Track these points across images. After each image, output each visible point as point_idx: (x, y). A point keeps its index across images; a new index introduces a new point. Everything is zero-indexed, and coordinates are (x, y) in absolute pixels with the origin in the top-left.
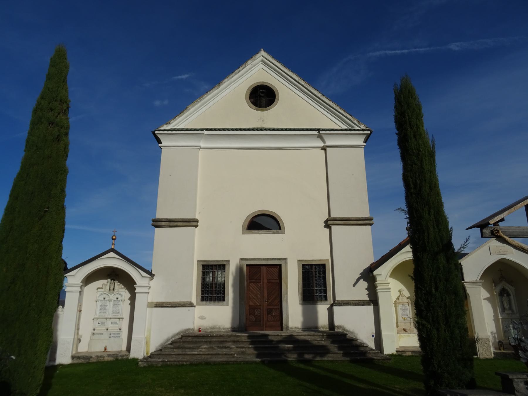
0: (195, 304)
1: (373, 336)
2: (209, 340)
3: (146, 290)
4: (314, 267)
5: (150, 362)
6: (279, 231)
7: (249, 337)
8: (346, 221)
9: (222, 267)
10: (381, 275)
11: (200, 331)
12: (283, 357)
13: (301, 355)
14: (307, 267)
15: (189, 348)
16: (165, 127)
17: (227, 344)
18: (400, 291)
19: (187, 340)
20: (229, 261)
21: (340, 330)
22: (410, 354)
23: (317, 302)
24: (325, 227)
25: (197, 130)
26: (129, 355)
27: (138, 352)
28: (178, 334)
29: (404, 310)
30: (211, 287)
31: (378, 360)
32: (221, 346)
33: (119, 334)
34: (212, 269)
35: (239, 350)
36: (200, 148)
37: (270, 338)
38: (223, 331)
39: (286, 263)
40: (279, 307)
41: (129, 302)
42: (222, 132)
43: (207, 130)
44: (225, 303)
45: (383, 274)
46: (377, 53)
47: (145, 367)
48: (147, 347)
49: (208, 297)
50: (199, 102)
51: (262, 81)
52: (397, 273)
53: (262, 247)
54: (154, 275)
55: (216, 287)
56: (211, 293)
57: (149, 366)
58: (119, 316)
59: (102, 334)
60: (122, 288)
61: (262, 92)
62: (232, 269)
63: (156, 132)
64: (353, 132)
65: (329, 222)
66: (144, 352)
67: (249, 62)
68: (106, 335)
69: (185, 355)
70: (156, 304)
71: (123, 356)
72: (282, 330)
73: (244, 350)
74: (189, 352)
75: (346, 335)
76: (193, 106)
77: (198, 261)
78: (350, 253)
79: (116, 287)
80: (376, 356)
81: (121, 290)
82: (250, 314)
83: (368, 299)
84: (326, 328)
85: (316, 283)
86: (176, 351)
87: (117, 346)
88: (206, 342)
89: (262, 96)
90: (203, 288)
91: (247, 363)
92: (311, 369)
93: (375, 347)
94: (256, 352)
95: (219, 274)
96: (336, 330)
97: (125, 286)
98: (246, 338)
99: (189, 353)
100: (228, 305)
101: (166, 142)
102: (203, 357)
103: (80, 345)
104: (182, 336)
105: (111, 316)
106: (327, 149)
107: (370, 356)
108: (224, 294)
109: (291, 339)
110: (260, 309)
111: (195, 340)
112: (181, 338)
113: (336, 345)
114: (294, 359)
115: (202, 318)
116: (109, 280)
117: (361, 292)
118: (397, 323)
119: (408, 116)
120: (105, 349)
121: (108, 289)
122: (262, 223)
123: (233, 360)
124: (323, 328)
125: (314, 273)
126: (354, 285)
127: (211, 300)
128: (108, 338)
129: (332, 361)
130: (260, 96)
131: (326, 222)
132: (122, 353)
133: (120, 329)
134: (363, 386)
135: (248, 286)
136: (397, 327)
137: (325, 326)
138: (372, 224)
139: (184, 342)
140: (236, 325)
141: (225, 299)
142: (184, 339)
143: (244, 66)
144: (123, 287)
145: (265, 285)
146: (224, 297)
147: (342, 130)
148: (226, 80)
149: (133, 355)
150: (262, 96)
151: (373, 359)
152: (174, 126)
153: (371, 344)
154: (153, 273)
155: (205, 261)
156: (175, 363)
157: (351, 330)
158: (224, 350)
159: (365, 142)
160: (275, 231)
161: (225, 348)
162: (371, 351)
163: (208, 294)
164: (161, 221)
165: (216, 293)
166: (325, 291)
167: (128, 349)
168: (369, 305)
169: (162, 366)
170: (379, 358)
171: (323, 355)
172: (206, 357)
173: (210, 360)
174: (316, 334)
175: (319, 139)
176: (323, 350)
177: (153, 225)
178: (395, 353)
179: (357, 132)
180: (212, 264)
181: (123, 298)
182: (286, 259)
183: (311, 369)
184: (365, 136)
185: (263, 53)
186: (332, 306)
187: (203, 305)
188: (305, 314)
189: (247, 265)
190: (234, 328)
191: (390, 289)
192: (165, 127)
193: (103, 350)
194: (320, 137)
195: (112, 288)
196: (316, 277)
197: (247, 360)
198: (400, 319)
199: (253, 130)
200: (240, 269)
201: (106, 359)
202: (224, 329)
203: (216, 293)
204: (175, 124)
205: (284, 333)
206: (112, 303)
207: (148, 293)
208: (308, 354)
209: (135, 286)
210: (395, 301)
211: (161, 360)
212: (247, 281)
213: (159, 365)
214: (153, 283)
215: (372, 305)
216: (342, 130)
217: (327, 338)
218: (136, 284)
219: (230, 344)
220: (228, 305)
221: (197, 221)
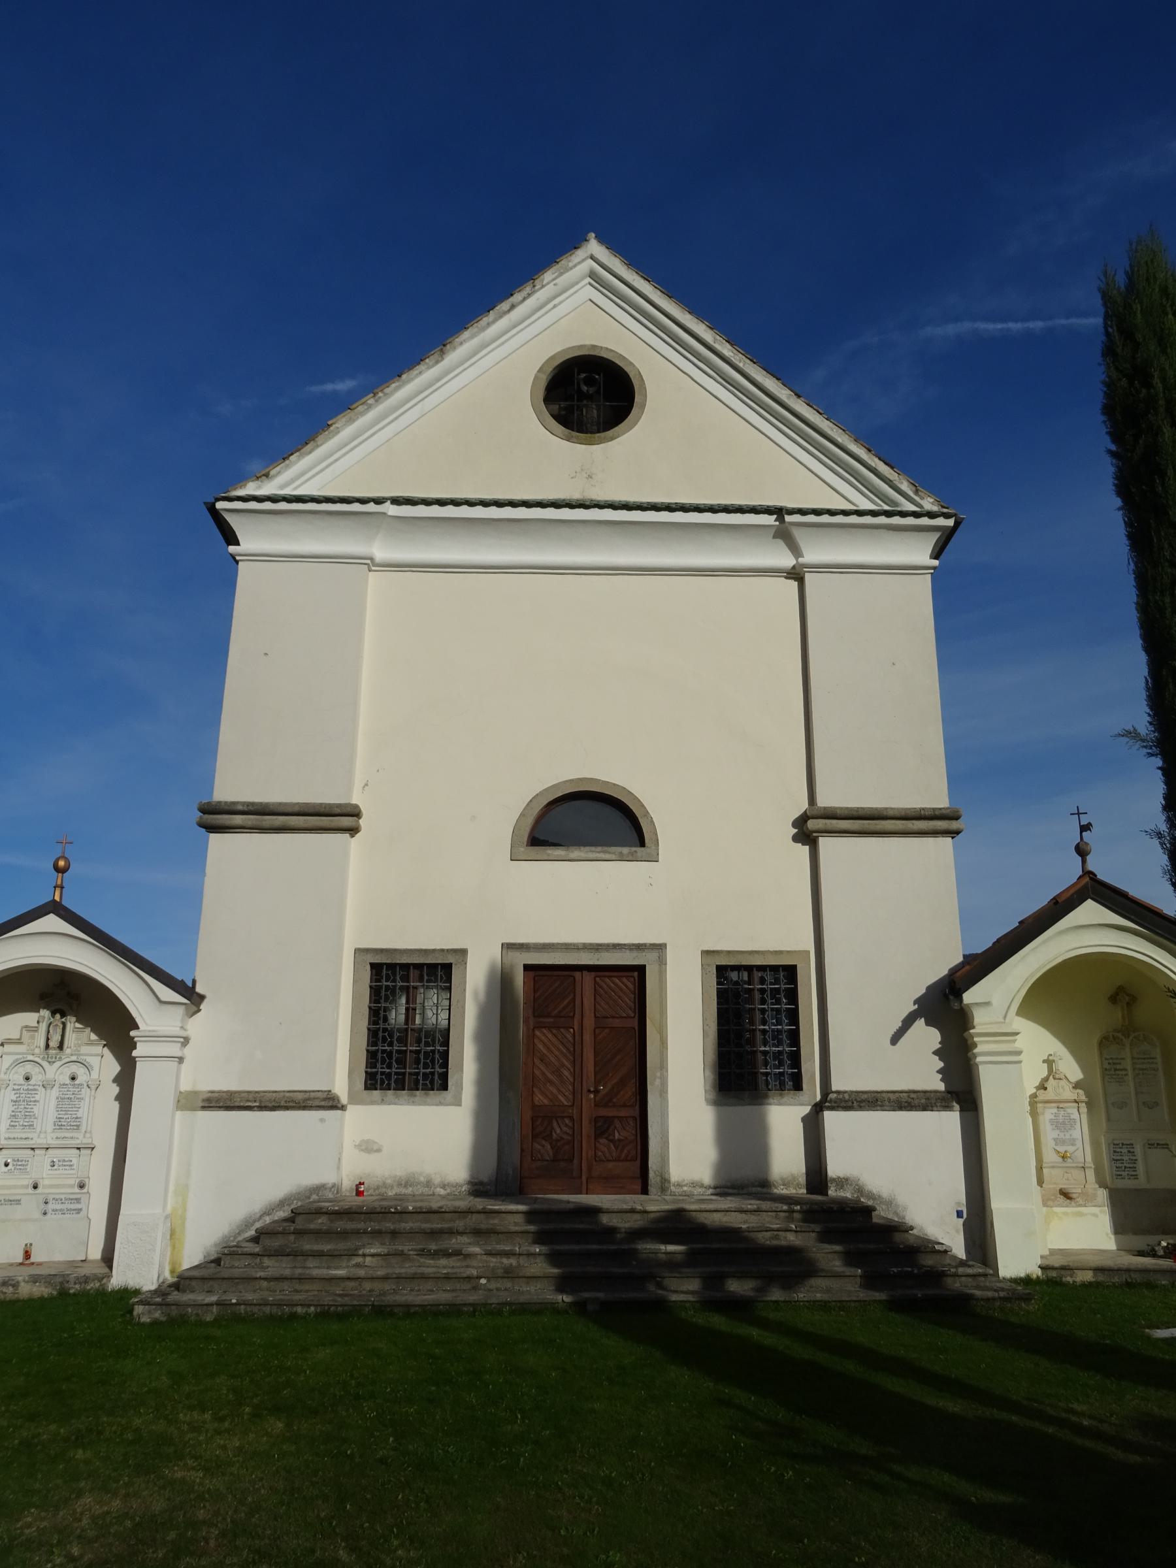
0: (344, 1099)
1: (959, 1214)
2: (390, 1226)
3: (174, 1049)
4: (757, 975)
5: (177, 1304)
6: (639, 850)
7: (531, 1216)
8: (868, 822)
9: (438, 972)
10: (988, 1004)
11: (359, 1193)
12: (651, 1287)
13: (713, 1281)
14: (734, 976)
15: (319, 1254)
16: (251, 489)
17: (455, 1242)
18: (1049, 1062)
19: (312, 1226)
20: (464, 952)
21: (847, 1194)
22: (1088, 1276)
23: (766, 1096)
24: (796, 838)
25: (363, 501)
26: (109, 1276)
27: (140, 1269)
28: (281, 1204)
29: (1062, 1125)
30: (403, 1040)
31: (988, 1300)
32: (433, 1247)
33: (78, 1200)
34: (406, 978)
35: (493, 1261)
36: (370, 563)
37: (605, 1219)
38: (442, 1192)
39: (662, 962)
40: (635, 1112)
41: (115, 1089)
42: (450, 511)
43: (396, 501)
44: (448, 1095)
45: (995, 1002)
46: (952, 329)
47: (155, 1323)
48: (174, 1247)
49: (389, 1075)
50: (370, 407)
51: (588, 342)
52: (1049, 998)
53: (581, 906)
54: (202, 998)
55: (419, 1041)
56: (401, 1062)
57: (172, 1321)
58: (80, 1139)
59: (18, 1202)
60: (91, 1043)
61: (589, 382)
62: (474, 980)
63: (220, 505)
64: (896, 520)
65: (812, 824)
66: (161, 1267)
67: (548, 276)
68: (31, 1206)
69: (300, 1279)
70: (208, 1100)
71: (86, 1280)
72: (645, 1191)
73: (513, 1261)
74: (317, 1269)
75: (868, 1211)
76: (351, 421)
77: (358, 952)
78: (883, 929)
79: (71, 1038)
80: (978, 1287)
81: (85, 1049)
82: (534, 1137)
83: (941, 1087)
84: (798, 1186)
85: (764, 1032)
86: (274, 1267)
87: (68, 1244)
88: (377, 1234)
89: (590, 394)
90: (374, 1044)
91: (523, 1309)
92: (755, 1333)
93: (967, 1251)
94: (556, 1271)
95: (431, 997)
96: (832, 1192)
97: (101, 1036)
98: (519, 1219)
99: (315, 1272)
100: (458, 1102)
101: (252, 539)
102: (368, 1286)
104: (295, 1213)
105: (50, 1140)
106: (808, 577)
107: (956, 1285)
108: (445, 1064)
109: (676, 1224)
110: (571, 1118)
111: (341, 1225)
112: (290, 1220)
113: (838, 1248)
114: (691, 1298)
115: (368, 1147)
116: (45, 1013)
117: (919, 1062)
118: (1040, 1169)
119: (1164, 379)
120: (27, 1255)
121: (42, 1044)
122: (588, 820)
123: (472, 1298)
124: (786, 1184)
125: (757, 996)
126: (895, 1040)
127: (400, 1086)
128: (37, 1214)
129: (824, 1306)
130: (582, 396)
131: (800, 822)
132: (86, 1271)
133: (82, 1186)
134: (954, 1406)
135: (530, 1037)
136: (1040, 1182)
137: (794, 1178)
138: (958, 832)
139: (299, 1233)
140: (488, 1171)
141: (451, 1082)
142: (300, 1223)
143: (528, 289)
144: (93, 1037)
145: (588, 1037)
146: (444, 1078)
147: (860, 513)
148: (466, 334)
149: (119, 1278)
151: (969, 1298)
152: (282, 487)
153: (955, 1242)
154: (199, 989)
155: (382, 951)
156: (267, 1309)
157: (885, 1193)
158: (443, 1262)
159: (936, 555)
160: (625, 850)
161: (447, 1254)
162: (961, 1270)
163: (389, 1066)
164: (230, 809)
165: (417, 1062)
166: (796, 1059)
167: (108, 1258)
168: (947, 1108)
169: (217, 1322)
170: (990, 1294)
171: (791, 1281)
172: (378, 1286)
173: (391, 1299)
174: (765, 1205)
175: (780, 543)
176: (789, 1266)
177: (202, 825)
178: (1037, 1272)
179: (910, 521)
180: (405, 960)
181: (95, 1075)
182: (660, 948)
183: (755, 1333)
184: (937, 535)
185: (594, 246)
186: (818, 1108)
187: (372, 1103)
188: (725, 1136)
189: (527, 968)
190: (481, 1183)
191: (1019, 1053)
192: (251, 489)
193: (20, 1258)
194: (784, 535)
195: (54, 1043)
196: (763, 1011)
197: (522, 1299)
198: (1050, 1156)
199: (556, 505)
200: (502, 981)
201: (26, 1290)
202: (444, 1186)
203: (417, 1062)
204: (286, 479)
205: (655, 1204)
206: (55, 1093)
207: (181, 1060)
208: (742, 1276)
209: (132, 1033)
210: (1034, 1096)
211: (214, 1299)
212: (526, 1021)
213: (209, 1318)
214: (197, 1026)
215: (957, 1107)
216: (860, 513)
217: (805, 1220)
218: (137, 1027)
219: (464, 1239)
220: (458, 1102)
221: (355, 813)
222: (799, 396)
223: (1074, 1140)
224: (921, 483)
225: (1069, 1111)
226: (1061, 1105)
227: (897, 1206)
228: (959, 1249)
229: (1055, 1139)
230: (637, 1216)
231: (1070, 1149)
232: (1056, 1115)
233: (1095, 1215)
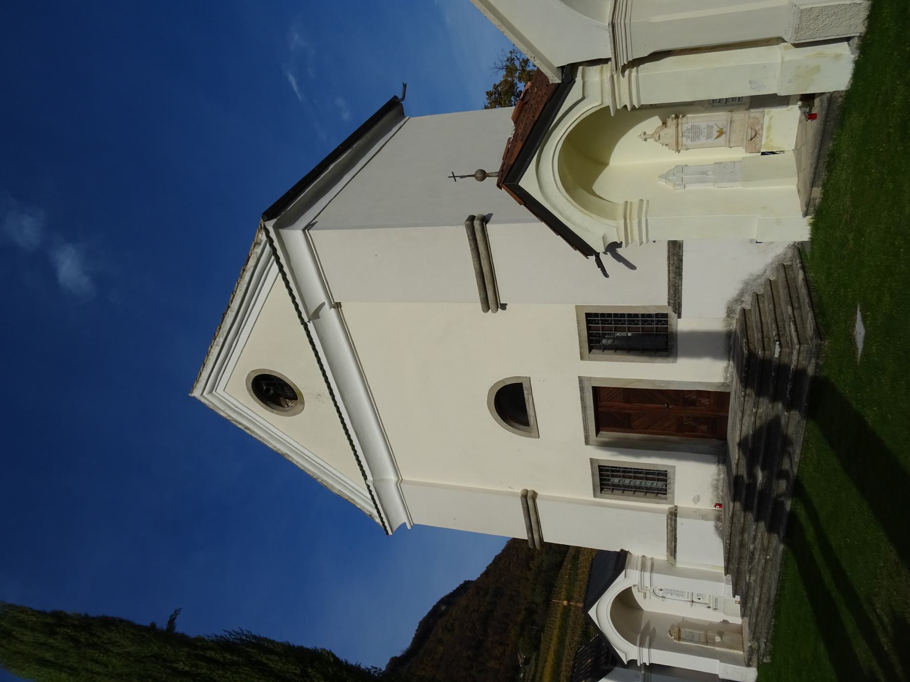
16: (378, 520)
23: (672, 333)
36: (399, 482)
43: (366, 478)
44: (669, 471)
53: (560, 408)
89: (272, 390)
101: (400, 518)
122: (512, 404)
126: (632, 267)
155: (594, 489)
157: (740, 286)
180: (585, 333)
185: (196, 393)
189: (598, 431)
194: (316, 315)
200: (605, 445)
202: (719, 475)
204: (369, 509)
222: (229, 307)
223: (708, 126)
224: (252, 242)
225: (684, 129)
226: (680, 135)
227: (749, 279)
229: (707, 138)
230: (741, 461)
231: (716, 129)
232: (688, 137)
233: (771, 118)
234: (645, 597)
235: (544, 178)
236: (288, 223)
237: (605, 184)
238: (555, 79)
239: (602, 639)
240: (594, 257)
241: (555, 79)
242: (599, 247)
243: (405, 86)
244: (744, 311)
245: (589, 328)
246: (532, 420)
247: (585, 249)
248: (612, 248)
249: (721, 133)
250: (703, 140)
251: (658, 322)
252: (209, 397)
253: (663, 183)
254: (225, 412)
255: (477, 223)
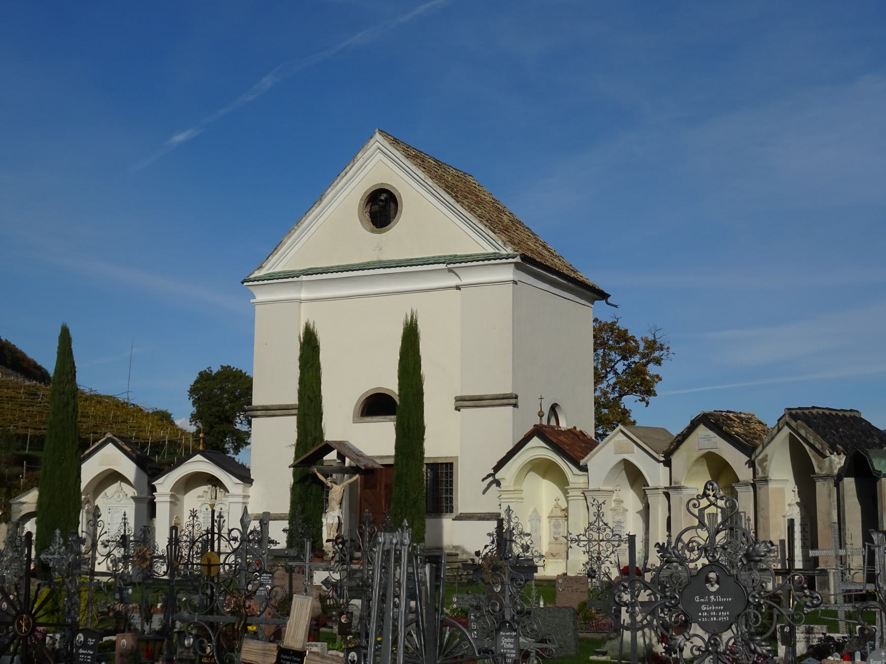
16: (257, 274)
36: (300, 301)
43: (307, 273)
67: (359, 155)
76: (289, 238)
89: (381, 208)
103: (684, 652)
126: (484, 492)
150: (381, 208)
180: (440, 462)
204: (277, 264)
214: (252, 490)
228: (34, 519)
234: (199, 497)
235: (537, 449)
236: (517, 266)
237: (533, 477)
238: (582, 462)
239: (171, 466)
240: (492, 472)
241: (582, 462)
242: (497, 476)
243: (616, 306)
244: (457, 555)
245: (442, 464)
246: (369, 419)
247: (497, 468)
248: (498, 484)
249: (556, 539)
250: (553, 530)
251: (447, 507)
252: (375, 146)
253: (532, 509)
254: (361, 157)
255: (513, 401)
